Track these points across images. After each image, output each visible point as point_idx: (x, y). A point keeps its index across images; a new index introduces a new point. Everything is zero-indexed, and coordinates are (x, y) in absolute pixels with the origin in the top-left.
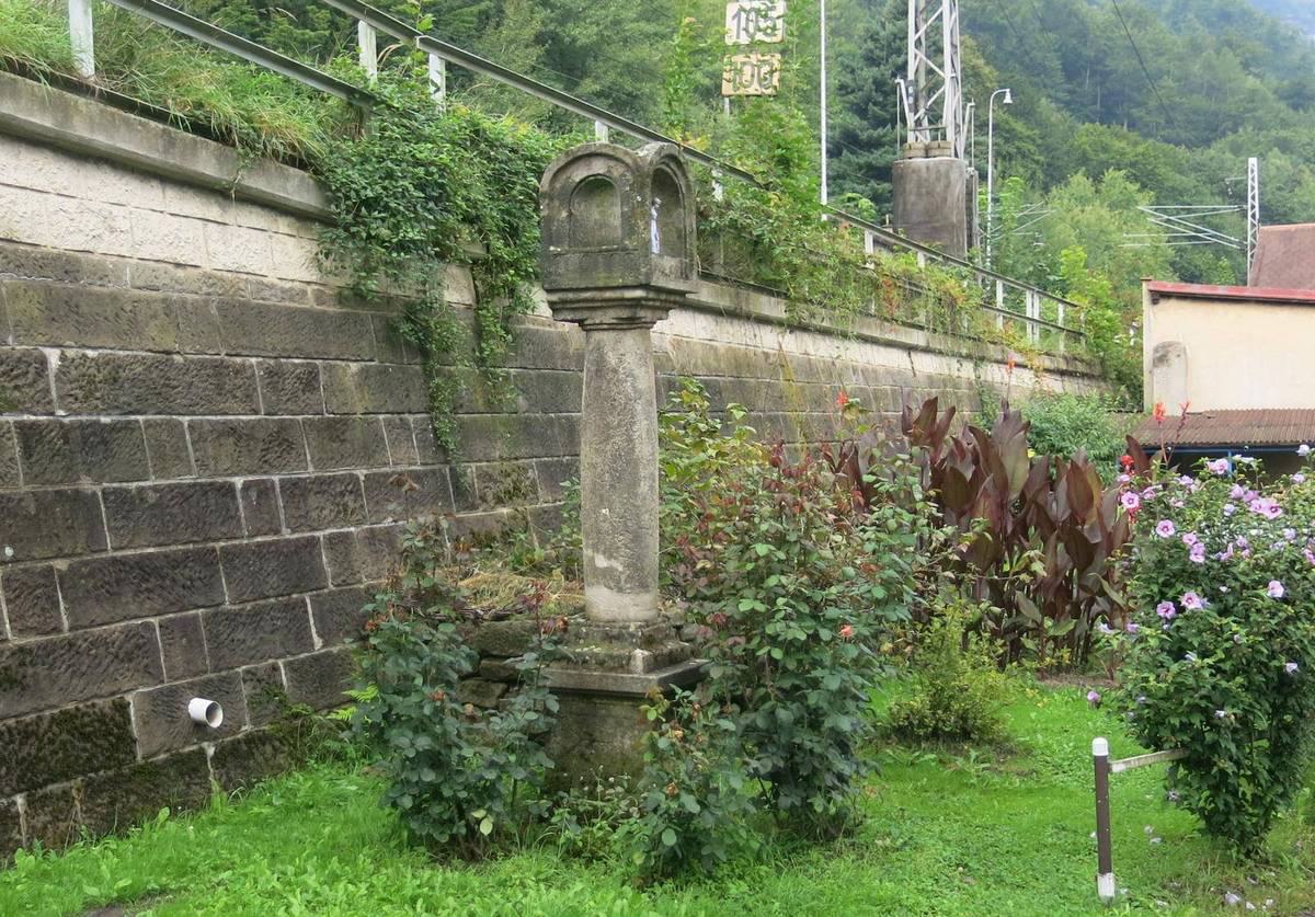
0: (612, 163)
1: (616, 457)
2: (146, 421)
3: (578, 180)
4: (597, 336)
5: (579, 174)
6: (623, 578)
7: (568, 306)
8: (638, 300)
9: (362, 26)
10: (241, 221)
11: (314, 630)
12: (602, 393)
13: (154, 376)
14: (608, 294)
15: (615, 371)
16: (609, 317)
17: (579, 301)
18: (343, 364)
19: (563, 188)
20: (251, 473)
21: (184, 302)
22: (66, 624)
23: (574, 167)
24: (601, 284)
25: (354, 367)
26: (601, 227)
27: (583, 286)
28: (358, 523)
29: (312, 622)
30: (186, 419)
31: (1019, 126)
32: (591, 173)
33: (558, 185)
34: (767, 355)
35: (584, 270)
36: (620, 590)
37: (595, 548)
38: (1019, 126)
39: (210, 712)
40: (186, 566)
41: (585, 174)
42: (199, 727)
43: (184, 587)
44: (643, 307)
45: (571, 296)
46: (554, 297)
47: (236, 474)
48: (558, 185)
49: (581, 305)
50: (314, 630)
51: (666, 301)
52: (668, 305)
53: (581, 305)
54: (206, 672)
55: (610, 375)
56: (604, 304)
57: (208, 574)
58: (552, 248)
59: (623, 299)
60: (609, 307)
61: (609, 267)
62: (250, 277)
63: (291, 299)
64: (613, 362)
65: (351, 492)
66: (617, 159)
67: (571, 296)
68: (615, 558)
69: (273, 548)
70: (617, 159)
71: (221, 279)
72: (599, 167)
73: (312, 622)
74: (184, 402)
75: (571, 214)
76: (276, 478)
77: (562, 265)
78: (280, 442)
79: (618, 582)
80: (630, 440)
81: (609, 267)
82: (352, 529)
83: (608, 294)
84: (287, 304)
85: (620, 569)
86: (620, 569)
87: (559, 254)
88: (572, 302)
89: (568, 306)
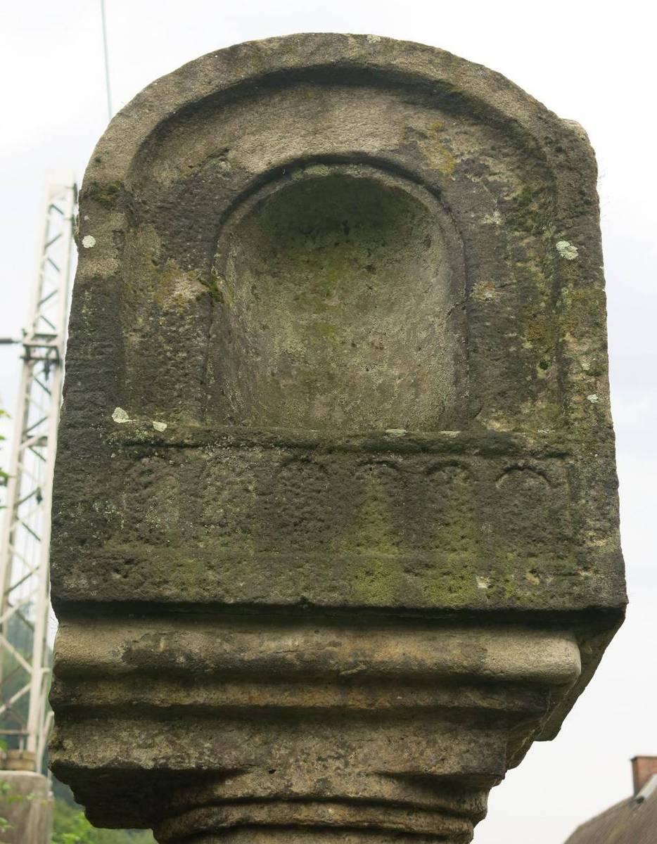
0: (422, 120)
3: (258, 165)
14: (399, 649)
17: (228, 674)
19: (188, 186)
22: (31, 774)
23: (249, 116)
24: (377, 593)
26: (309, 387)
27: (280, 594)
31: (284, 766)
32: (324, 146)
33: (165, 175)
35: (278, 524)
38: (284, 766)
41: (296, 148)
45: (195, 643)
46: (106, 646)
48: (165, 175)
49: (235, 695)
53: (235, 695)
56: (357, 700)
58: (120, 416)
60: (375, 719)
61: (415, 520)
67: (195, 643)
75: (211, 299)
77: (169, 487)
81: (415, 520)
83: (399, 649)
87: (158, 445)
88: (187, 676)
89: (161, 696)
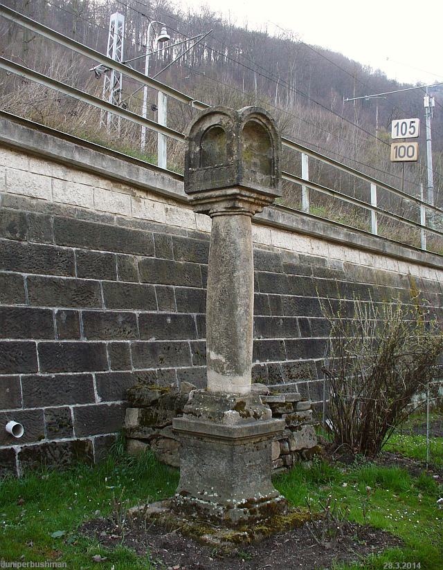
0: (222, 117)
1: (223, 292)
2: (141, 315)
3: (205, 129)
4: (217, 219)
5: (206, 125)
6: (225, 366)
7: (199, 202)
8: (235, 194)
9: (160, 95)
10: (75, 180)
11: (96, 392)
12: (217, 254)
13: (8, 251)
15: (224, 240)
16: (220, 207)
17: (204, 199)
18: (133, 256)
20: (63, 306)
21: (32, 216)
25: (140, 258)
28: (132, 338)
29: (95, 388)
30: (25, 275)
33: (195, 134)
34: (401, 276)
36: (223, 373)
37: (211, 349)
39: (16, 429)
40: (13, 351)
42: (10, 438)
43: (11, 361)
44: (240, 200)
45: (200, 195)
47: (55, 306)
50: (96, 392)
51: (264, 201)
52: (264, 203)
54: (20, 408)
55: (222, 243)
57: (29, 355)
59: (226, 196)
62: (77, 207)
63: (103, 221)
64: (223, 234)
65: (129, 322)
66: (224, 114)
67: (200, 195)
68: (221, 354)
69: (73, 346)
70: (224, 114)
71: (59, 207)
72: (215, 120)
73: (95, 388)
74: (26, 266)
76: (80, 310)
78: (85, 293)
79: (223, 368)
80: (231, 282)
82: (129, 341)
84: (100, 223)
85: (224, 360)
86: (224, 360)
89: (199, 202)
